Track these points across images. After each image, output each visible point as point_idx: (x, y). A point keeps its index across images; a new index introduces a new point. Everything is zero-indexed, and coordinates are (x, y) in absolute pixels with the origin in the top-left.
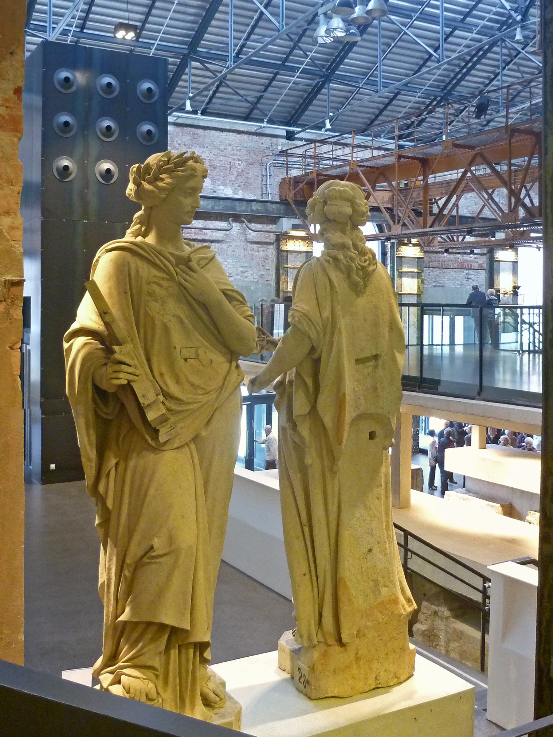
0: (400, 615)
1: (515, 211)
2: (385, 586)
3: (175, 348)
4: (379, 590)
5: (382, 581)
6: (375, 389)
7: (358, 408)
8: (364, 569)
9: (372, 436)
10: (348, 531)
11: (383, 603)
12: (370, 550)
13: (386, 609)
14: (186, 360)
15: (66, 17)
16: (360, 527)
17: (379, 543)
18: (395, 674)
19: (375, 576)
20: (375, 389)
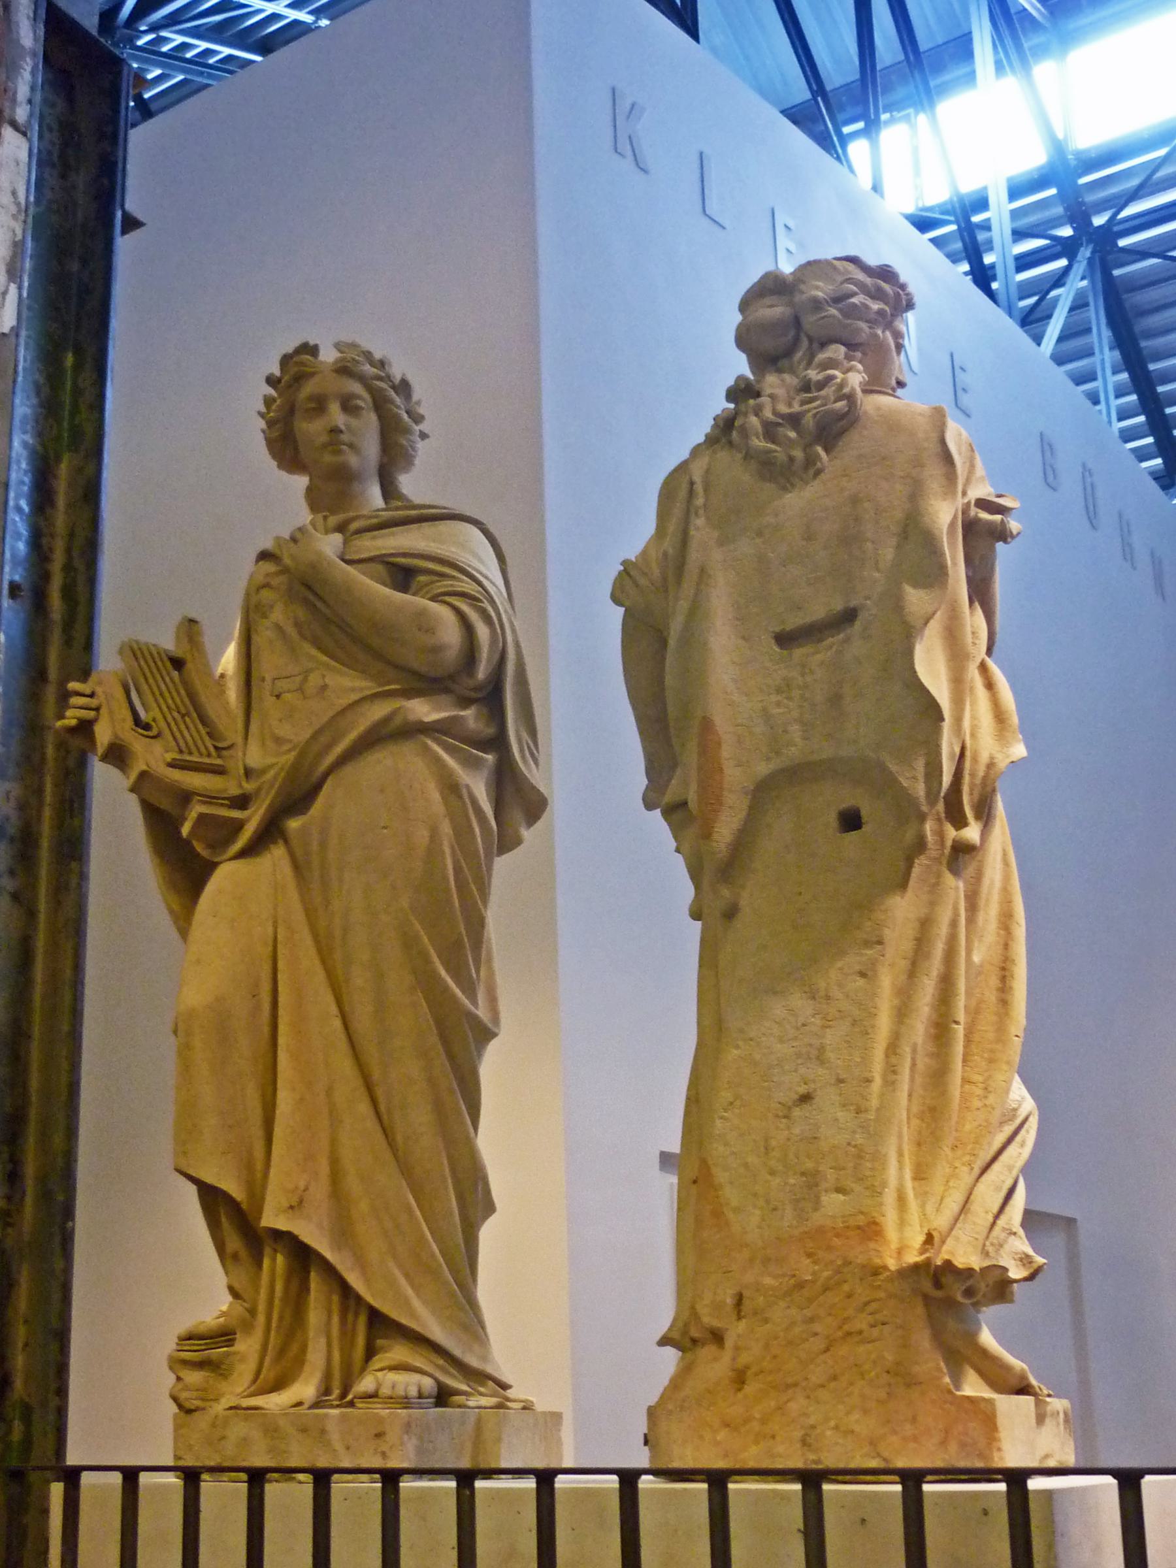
0: (877, 1271)
1: (949, 207)
2: (839, 1190)
3: (263, 680)
4: (818, 1197)
5: (831, 1175)
6: (835, 700)
7: (778, 753)
8: (773, 1143)
9: (851, 821)
10: (737, 1047)
11: (821, 1230)
12: (806, 1098)
13: (829, 1248)
14: (278, 696)
15: (1011, 265)
16: (781, 1040)
17: (841, 1081)
18: (717, 1337)
19: (809, 1165)
20: (835, 700)
